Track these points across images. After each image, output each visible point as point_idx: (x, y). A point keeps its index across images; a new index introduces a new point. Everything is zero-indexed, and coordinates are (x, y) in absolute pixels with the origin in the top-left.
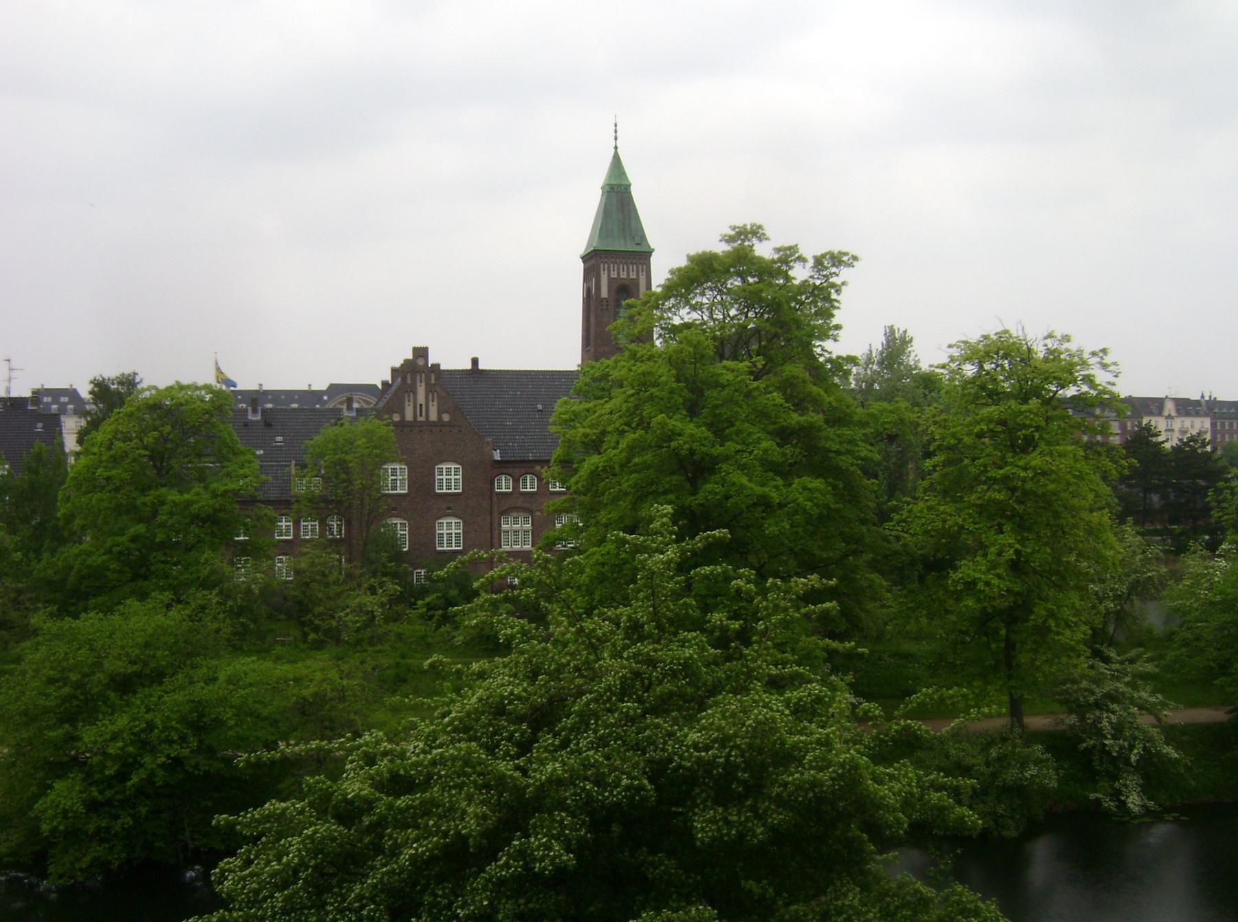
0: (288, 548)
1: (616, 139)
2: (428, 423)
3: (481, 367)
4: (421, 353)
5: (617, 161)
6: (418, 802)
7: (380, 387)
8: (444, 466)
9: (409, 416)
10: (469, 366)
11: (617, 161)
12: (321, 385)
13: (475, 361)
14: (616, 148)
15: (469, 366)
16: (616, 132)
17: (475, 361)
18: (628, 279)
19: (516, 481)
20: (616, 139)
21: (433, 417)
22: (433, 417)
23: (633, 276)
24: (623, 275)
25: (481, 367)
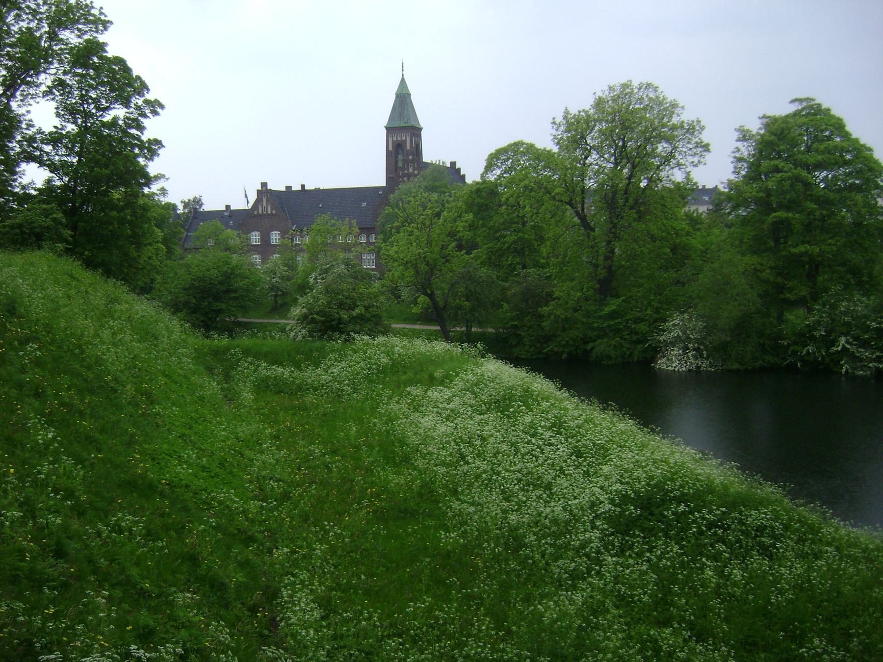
0: (86, 255)
2: (267, 215)
3: (306, 188)
4: (264, 185)
5: (403, 80)
6: (250, 359)
7: (555, 149)
8: (274, 233)
9: (260, 212)
10: (300, 189)
11: (403, 80)
12: (506, 145)
13: (303, 186)
15: (300, 189)
17: (303, 186)
18: (402, 141)
19: (368, 237)
21: (269, 212)
22: (269, 212)
23: (404, 138)
24: (399, 139)
25: (306, 188)
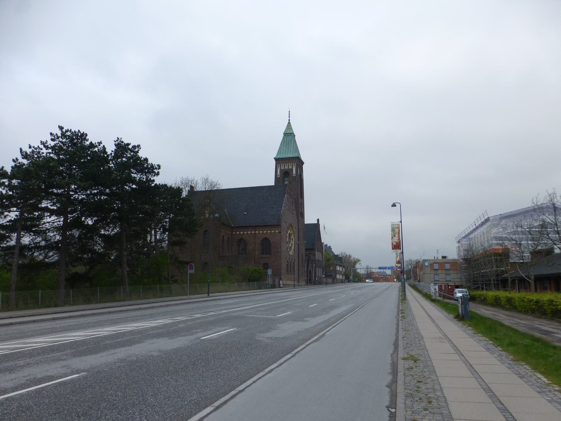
1: (289, 117)
14: (289, 120)
16: (289, 114)
20: (289, 117)
23: (290, 167)
24: (286, 168)
